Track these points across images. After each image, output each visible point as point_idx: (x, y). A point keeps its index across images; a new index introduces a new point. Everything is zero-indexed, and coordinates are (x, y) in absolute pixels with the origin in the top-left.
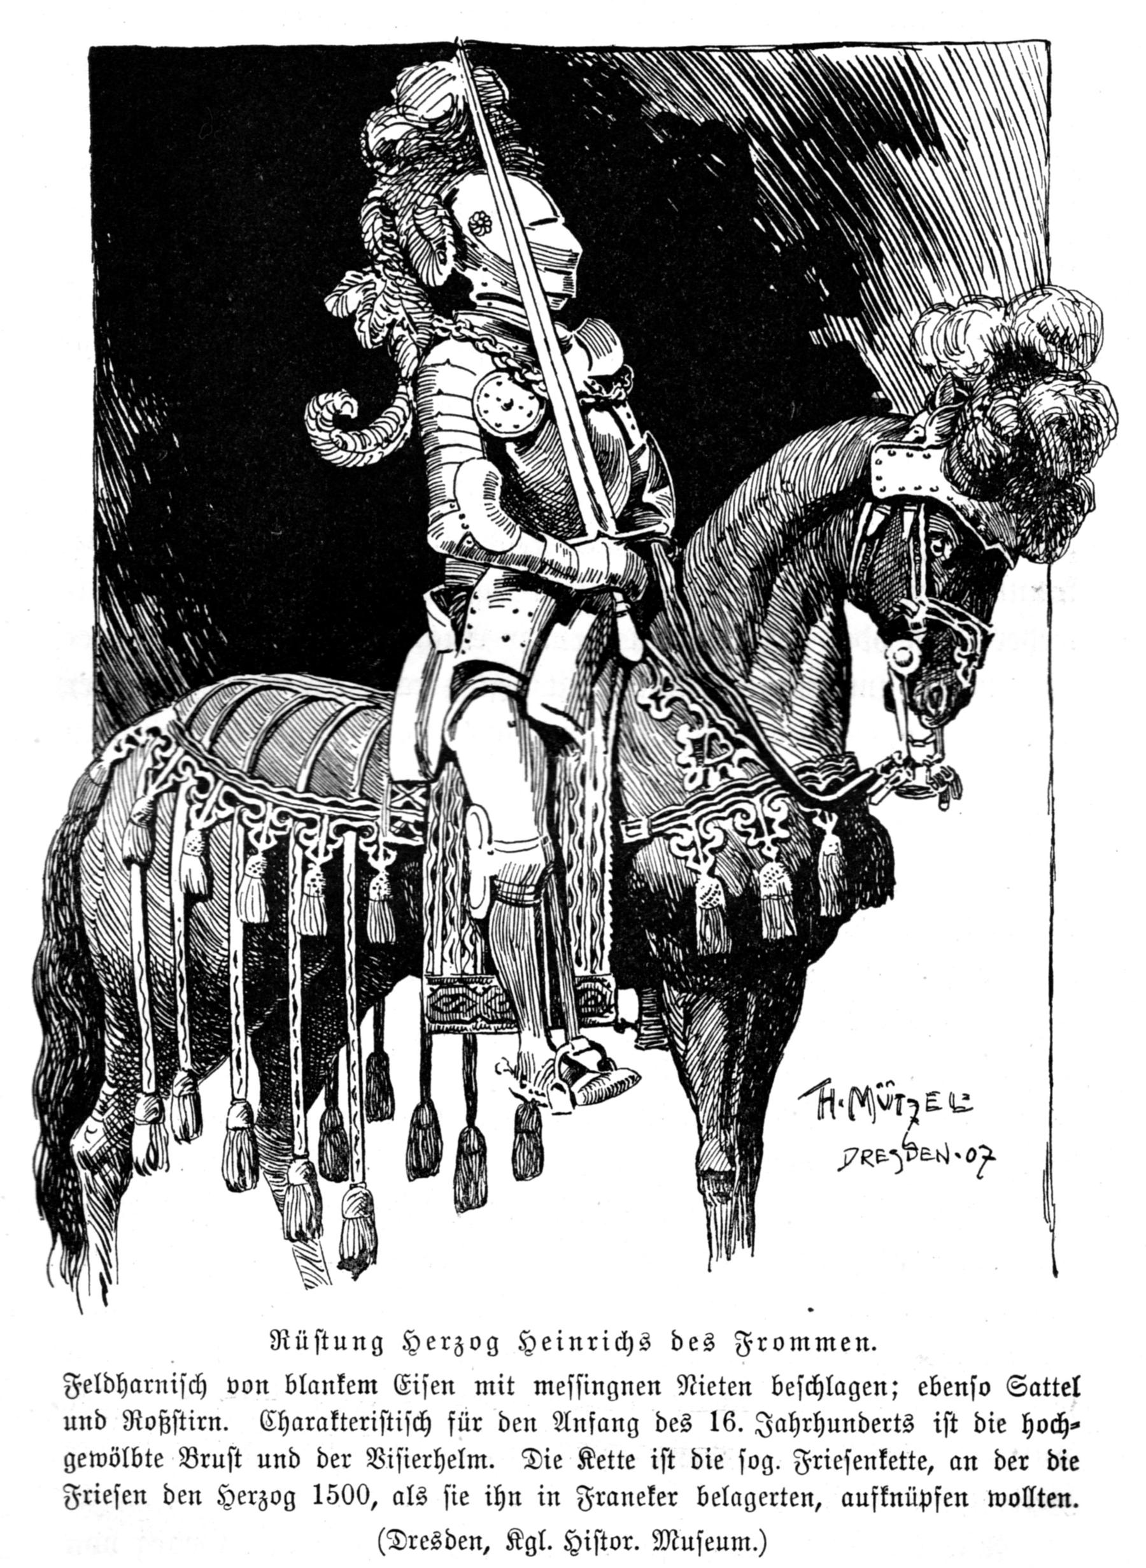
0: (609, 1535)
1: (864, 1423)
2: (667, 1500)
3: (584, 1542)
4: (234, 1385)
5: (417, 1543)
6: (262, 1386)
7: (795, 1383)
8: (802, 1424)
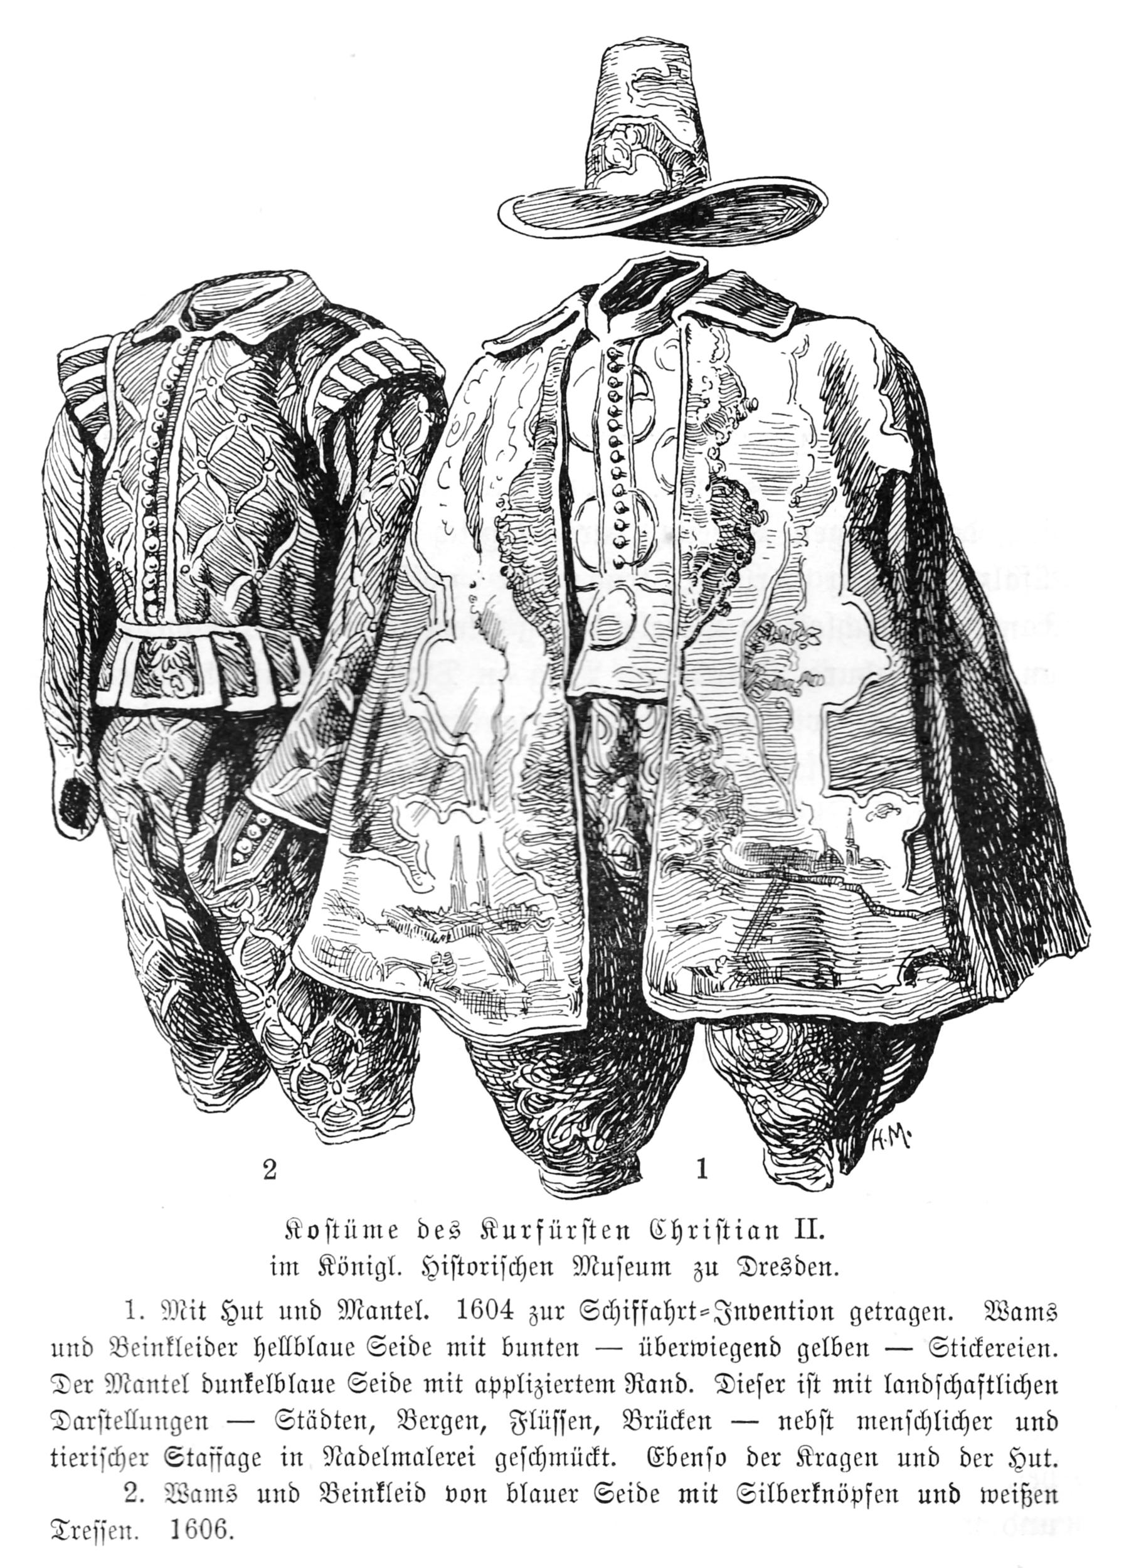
0: (465, 1261)
1: (364, 1456)
2: (775, 1387)
3: (441, 1267)
4: (452, 1493)
5: (767, 1269)
6: (480, 1494)
7: (519, 1454)
8: (677, 1311)
